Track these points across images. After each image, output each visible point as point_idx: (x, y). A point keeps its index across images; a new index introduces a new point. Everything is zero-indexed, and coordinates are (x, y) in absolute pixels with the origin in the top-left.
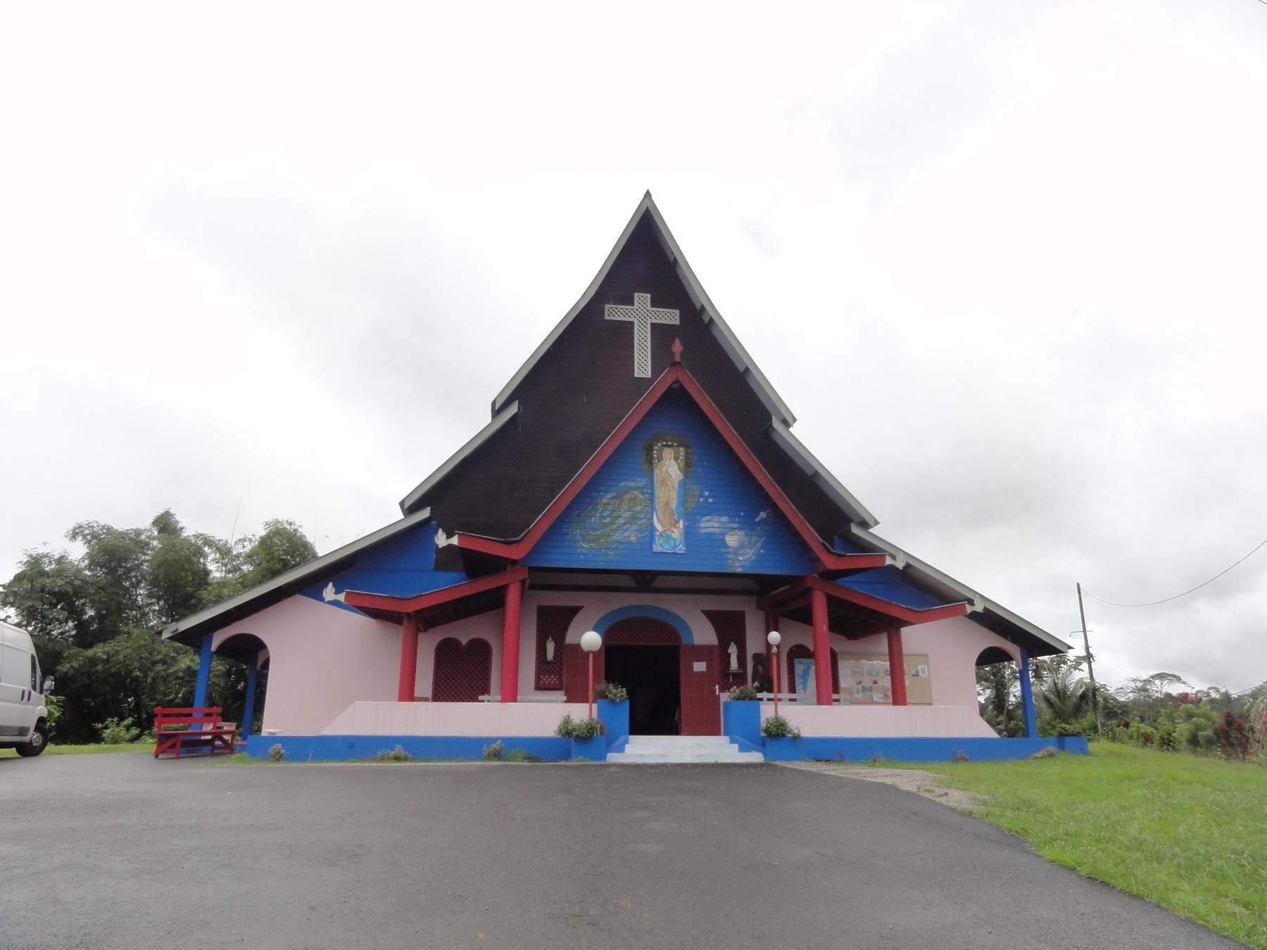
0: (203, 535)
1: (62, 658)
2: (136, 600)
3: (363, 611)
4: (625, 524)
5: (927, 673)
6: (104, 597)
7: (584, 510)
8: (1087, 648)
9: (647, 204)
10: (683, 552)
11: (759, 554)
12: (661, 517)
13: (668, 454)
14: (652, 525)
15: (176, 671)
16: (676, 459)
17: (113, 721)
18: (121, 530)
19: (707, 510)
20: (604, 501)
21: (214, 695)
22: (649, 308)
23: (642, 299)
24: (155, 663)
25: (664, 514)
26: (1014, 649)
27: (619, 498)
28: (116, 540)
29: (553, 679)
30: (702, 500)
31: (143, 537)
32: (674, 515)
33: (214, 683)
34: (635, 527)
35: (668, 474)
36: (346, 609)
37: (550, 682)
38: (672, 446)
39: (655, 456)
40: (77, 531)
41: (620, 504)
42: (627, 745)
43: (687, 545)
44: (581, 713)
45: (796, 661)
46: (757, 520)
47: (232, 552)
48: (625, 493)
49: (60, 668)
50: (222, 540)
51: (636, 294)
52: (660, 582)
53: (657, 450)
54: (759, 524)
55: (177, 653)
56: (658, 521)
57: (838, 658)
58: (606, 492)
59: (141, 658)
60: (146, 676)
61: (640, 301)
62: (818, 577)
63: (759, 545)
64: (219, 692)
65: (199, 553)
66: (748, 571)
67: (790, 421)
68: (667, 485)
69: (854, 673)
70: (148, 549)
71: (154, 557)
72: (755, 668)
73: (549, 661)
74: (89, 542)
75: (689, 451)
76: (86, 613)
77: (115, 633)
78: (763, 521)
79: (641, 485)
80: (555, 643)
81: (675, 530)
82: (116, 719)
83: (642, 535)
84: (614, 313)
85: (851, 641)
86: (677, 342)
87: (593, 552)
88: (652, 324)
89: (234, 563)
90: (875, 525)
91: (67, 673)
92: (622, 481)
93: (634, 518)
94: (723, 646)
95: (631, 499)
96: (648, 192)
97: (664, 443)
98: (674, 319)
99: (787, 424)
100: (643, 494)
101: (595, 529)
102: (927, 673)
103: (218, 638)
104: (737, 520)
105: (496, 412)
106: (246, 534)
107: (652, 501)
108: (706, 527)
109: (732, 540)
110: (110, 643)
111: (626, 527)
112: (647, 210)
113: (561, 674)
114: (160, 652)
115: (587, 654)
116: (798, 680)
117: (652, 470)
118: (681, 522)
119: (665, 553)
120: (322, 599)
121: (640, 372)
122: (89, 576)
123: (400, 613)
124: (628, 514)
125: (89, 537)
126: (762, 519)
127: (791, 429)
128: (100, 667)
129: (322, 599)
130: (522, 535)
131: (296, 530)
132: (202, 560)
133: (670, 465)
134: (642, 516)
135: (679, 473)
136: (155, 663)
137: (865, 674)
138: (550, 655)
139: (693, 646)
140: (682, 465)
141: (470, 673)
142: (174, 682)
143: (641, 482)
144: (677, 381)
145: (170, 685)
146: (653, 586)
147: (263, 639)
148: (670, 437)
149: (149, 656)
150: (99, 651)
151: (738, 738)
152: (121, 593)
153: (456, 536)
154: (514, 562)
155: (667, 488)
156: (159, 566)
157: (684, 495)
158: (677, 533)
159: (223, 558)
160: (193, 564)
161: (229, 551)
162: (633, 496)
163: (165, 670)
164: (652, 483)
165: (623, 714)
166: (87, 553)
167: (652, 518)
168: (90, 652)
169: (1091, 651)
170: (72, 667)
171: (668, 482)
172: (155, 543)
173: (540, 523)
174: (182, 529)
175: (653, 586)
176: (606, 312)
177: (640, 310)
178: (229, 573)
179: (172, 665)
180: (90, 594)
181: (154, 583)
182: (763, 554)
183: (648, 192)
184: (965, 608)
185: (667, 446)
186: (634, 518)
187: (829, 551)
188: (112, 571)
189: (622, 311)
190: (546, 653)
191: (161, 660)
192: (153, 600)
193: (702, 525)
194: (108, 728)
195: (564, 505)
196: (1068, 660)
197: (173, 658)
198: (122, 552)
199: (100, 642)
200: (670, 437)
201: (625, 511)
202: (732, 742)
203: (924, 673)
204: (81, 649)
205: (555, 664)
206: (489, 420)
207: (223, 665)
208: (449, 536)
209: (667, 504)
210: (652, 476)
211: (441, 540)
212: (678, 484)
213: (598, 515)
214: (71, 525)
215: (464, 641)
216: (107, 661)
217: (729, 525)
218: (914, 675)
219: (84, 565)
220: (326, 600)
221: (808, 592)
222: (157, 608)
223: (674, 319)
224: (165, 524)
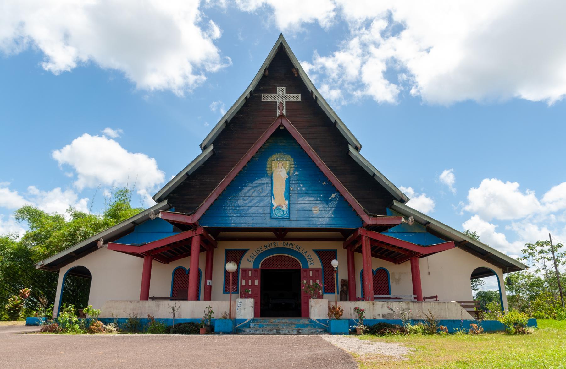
4: (256, 203)
10: (288, 217)
19: (301, 195)
20: (245, 191)
23: (281, 90)
30: (299, 189)
46: (330, 198)
58: (245, 188)
63: (331, 212)
84: (267, 98)
85: (397, 265)
88: (286, 101)
93: (261, 200)
98: (298, 99)
99: (357, 149)
104: (318, 199)
105: (204, 149)
109: (316, 210)
133: (281, 171)
176: (262, 98)
182: (333, 217)
223: (298, 99)
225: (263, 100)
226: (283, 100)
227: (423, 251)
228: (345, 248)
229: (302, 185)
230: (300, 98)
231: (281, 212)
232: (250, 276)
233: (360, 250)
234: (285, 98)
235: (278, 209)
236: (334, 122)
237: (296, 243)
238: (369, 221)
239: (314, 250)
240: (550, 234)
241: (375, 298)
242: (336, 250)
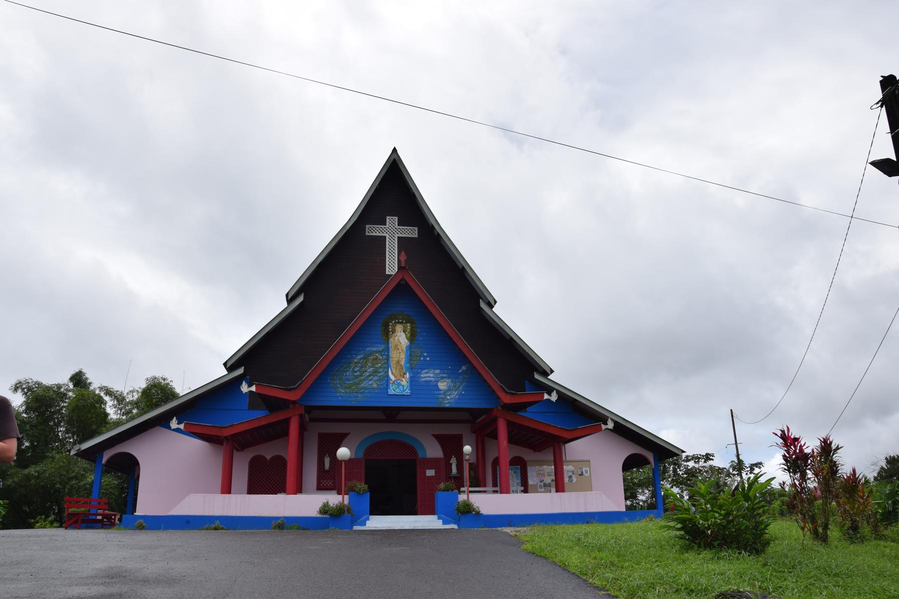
0: (105, 387)
1: (7, 475)
2: (58, 435)
3: (195, 435)
4: (369, 376)
5: (589, 473)
6: (36, 432)
7: (342, 367)
8: (738, 456)
9: (394, 156)
10: (409, 394)
12: (394, 371)
13: (399, 328)
14: (388, 376)
15: (85, 484)
16: (404, 331)
17: (41, 518)
18: (47, 385)
21: (111, 501)
23: (392, 221)
24: (70, 479)
25: (396, 369)
26: (650, 456)
27: (365, 359)
28: (44, 392)
29: (330, 483)
31: (62, 390)
32: (403, 369)
33: (111, 492)
34: (376, 378)
35: (399, 341)
36: (185, 434)
37: (327, 485)
38: (401, 323)
39: (390, 330)
40: (18, 386)
41: (366, 363)
42: (367, 521)
43: (411, 389)
44: (334, 499)
47: (126, 400)
48: (370, 355)
49: (6, 482)
50: (119, 391)
51: (388, 217)
52: (402, 415)
53: (391, 326)
54: (461, 374)
55: (85, 472)
56: (392, 373)
57: (528, 465)
58: (357, 355)
59: (61, 475)
60: (64, 488)
61: (390, 222)
62: (501, 408)
64: (115, 499)
65: (101, 401)
66: (453, 406)
67: (493, 303)
68: (398, 349)
69: (538, 475)
70: (66, 399)
71: (69, 404)
73: (327, 470)
74: (26, 394)
75: (414, 326)
76: (23, 445)
77: (43, 458)
78: (464, 372)
79: (381, 349)
80: (331, 458)
81: (403, 379)
82: (43, 517)
83: (381, 383)
84: (373, 231)
87: (348, 395)
88: (398, 237)
89: (127, 408)
90: (551, 374)
91: (10, 485)
93: (376, 372)
94: (447, 457)
95: (373, 359)
96: (395, 148)
97: (397, 321)
99: (491, 306)
100: (382, 355)
101: (349, 380)
102: (589, 473)
103: (107, 456)
105: (290, 300)
106: (135, 387)
107: (388, 360)
108: (425, 377)
109: (442, 385)
110: (40, 465)
111: (370, 378)
112: (394, 160)
113: (334, 479)
114: (74, 471)
115: (341, 461)
117: (388, 339)
118: (408, 374)
119: (396, 395)
120: (169, 428)
121: (390, 271)
122: (25, 417)
123: (220, 437)
124: (371, 369)
125: (26, 390)
128: (33, 482)
130: (297, 385)
131: (168, 384)
132: (103, 406)
133: (400, 336)
134: (381, 371)
135: (406, 341)
136: (70, 479)
137: (546, 474)
138: (327, 465)
139: (426, 458)
140: (409, 335)
141: (273, 475)
142: (83, 492)
143: (381, 347)
144: (403, 279)
145: (81, 494)
146: (397, 418)
147: (136, 457)
148: (401, 317)
149: (66, 474)
150: (32, 470)
151: (443, 516)
152: (47, 429)
153: (254, 386)
154: (294, 402)
155: (398, 351)
156: (73, 410)
157: (411, 355)
158: (404, 382)
159: (119, 404)
160: (96, 408)
161: (124, 399)
162: (375, 357)
163: (77, 484)
164: (388, 348)
166: (24, 402)
167: (388, 372)
168: (26, 471)
169: (741, 457)
170: (13, 481)
171: (399, 347)
172: (71, 394)
173: (310, 377)
174: (90, 384)
175: (397, 418)
176: (367, 230)
177: (390, 228)
178: (123, 416)
179: (82, 480)
180: (27, 430)
181: (70, 422)
182: (463, 395)
183: (395, 148)
184: (601, 426)
186: (375, 372)
188: (42, 414)
189: (374, 229)
190: (324, 465)
191: (74, 476)
192: (70, 435)
193: (422, 376)
194: (38, 523)
195: (325, 364)
196: (745, 467)
197: (83, 475)
198: (48, 401)
199: (33, 464)
200: (401, 317)
201: (370, 367)
202: (439, 519)
203: (587, 472)
204: (19, 469)
205: (331, 472)
206: (287, 306)
207: (117, 480)
208: (250, 386)
209: (398, 362)
211: (245, 388)
212: (406, 348)
213: (351, 370)
214: (14, 382)
215: (268, 457)
216: (37, 477)
217: (441, 375)
218: (580, 475)
219: (22, 410)
220: (172, 428)
221: (495, 420)
222: (72, 440)
224: (78, 379)
226: (394, 235)
227: (566, 435)
228: (474, 432)
229: (425, 354)
230: (416, 232)
231: (401, 387)
233: (494, 436)
234: (398, 232)
235: (397, 384)
236: (461, 268)
238: (507, 399)
239: (433, 435)
241: (471, 492)
242: (462, 435)
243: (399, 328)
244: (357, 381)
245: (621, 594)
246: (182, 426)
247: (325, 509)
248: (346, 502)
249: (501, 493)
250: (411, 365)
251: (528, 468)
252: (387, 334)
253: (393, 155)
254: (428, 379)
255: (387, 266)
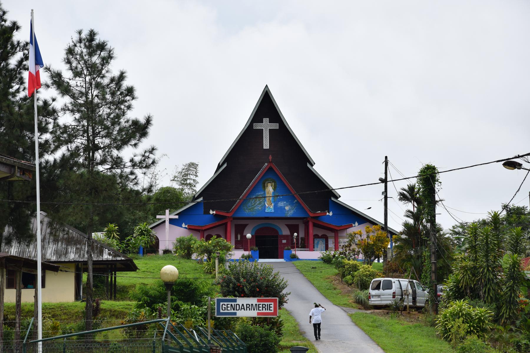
4: (258, 205)
11: (294, 212)
13: (269, 185)
14: (265, 205)
16: (272, 186)
22: (268, 123)
23: (266, 120)
34: (260, 205)
38: (270, 182)
43: (274, 210)
44: (246, 253)
45: (315, 239)
51: (264, 119)
54: (294, 203)
66: (291, 216)
67: (313, 164)
72: (301, 241)
84: (257, 126)
86: (270, 156)
88: (269, 129)
92: (257, 193)
93: (260, 203)
99: (312, 165)
101: (250, 207)
109: (287, 208)
116: (315, 245)
117: (265, 189)
126: (296, 202)
127: (313, 167)
129: (182, 227)
135: (272, 190)
138: (239, 239)
140: (273, 188)
158: (272, 207)
164: (265, 193)
165: (257, 253)
176: (254, 126)
185: (269, 182)
187: (311, 212)
210: (265, 191)
221: (308, 222)
225: (254, 128)
230: (278, 126)
232: (286, 242)
237: (217, 224)
238: (312, 215)
240: (32, 10)
243: (269, 185)
244: (253, 207)
245: (126, 218)
246: (187, 226)
247: (243, 256)
248: (250, 254)
249: (310, 251)
250: (274, 200)
251: (329, 240)
252: (264, 187)
253: (266, 88)
254: (281, 206)
255: (264, 144)
